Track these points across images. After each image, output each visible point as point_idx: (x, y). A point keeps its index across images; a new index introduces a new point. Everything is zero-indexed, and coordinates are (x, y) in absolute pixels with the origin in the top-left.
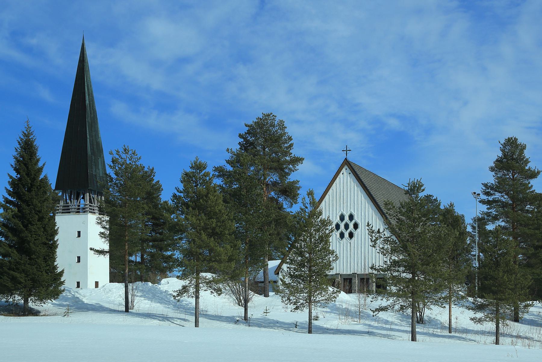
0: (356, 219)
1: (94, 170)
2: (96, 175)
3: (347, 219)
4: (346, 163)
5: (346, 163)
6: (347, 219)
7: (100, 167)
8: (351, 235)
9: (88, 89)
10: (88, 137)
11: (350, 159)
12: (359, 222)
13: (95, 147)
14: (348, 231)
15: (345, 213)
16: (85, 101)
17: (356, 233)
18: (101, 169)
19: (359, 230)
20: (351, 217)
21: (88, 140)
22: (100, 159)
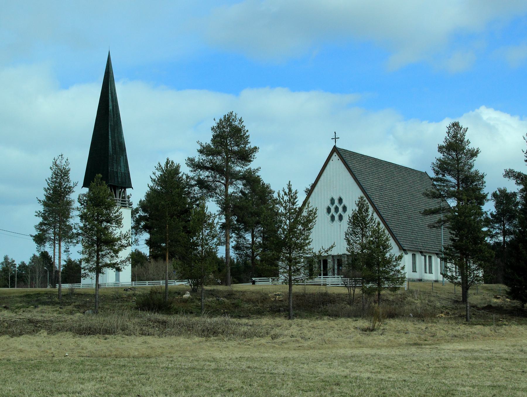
0: (345, 202)
1: (115, 167)
2: (117, 172)
3: (336, 203)
4: (335, 150)
5: (335, 150)
6: (336, 203)
7: (122, 164)
8: (332, 201)
9: (112, 97)
10: (110, 138)
11: (338, 146)
12: (347, 205)
13: (117, 147)
14: (334, 206)
15: (338, 223)
16: (108, 107)
17: (328, 203)
18: (123, 167)
19: (326, 206)
20: (340, 200)
21: (110, 141)
22: (122, 157)
